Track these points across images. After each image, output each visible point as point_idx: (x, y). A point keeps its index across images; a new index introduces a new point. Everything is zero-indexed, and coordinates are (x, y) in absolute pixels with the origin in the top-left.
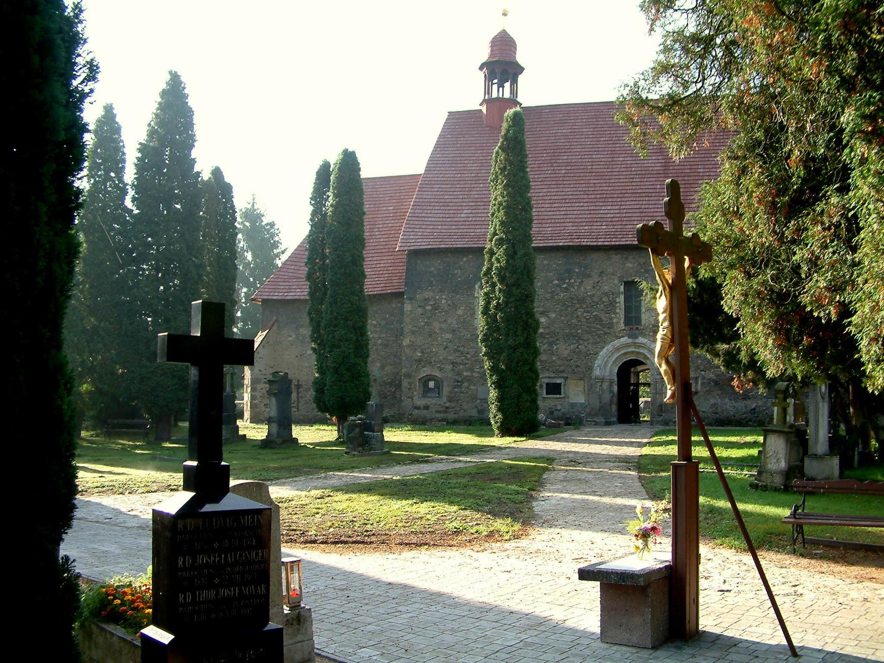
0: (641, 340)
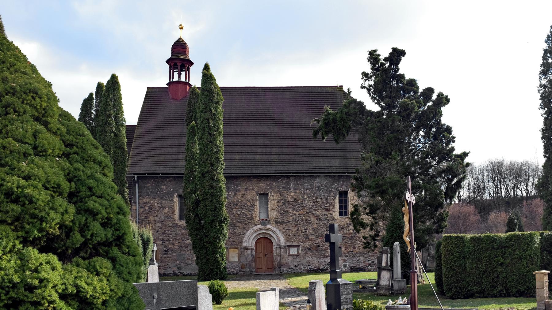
0: (269, 226)
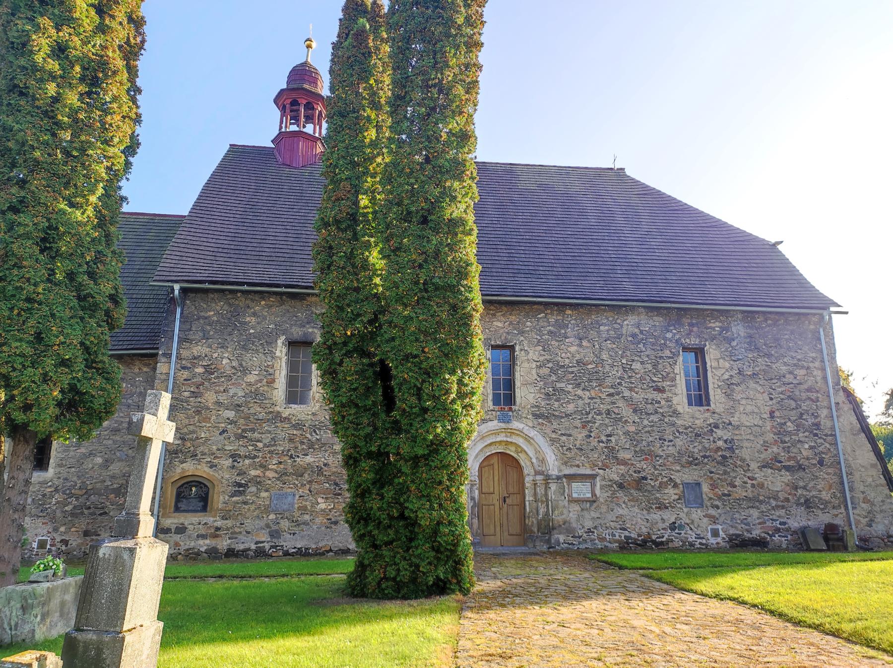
0: (516, 425)
